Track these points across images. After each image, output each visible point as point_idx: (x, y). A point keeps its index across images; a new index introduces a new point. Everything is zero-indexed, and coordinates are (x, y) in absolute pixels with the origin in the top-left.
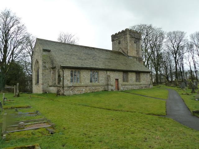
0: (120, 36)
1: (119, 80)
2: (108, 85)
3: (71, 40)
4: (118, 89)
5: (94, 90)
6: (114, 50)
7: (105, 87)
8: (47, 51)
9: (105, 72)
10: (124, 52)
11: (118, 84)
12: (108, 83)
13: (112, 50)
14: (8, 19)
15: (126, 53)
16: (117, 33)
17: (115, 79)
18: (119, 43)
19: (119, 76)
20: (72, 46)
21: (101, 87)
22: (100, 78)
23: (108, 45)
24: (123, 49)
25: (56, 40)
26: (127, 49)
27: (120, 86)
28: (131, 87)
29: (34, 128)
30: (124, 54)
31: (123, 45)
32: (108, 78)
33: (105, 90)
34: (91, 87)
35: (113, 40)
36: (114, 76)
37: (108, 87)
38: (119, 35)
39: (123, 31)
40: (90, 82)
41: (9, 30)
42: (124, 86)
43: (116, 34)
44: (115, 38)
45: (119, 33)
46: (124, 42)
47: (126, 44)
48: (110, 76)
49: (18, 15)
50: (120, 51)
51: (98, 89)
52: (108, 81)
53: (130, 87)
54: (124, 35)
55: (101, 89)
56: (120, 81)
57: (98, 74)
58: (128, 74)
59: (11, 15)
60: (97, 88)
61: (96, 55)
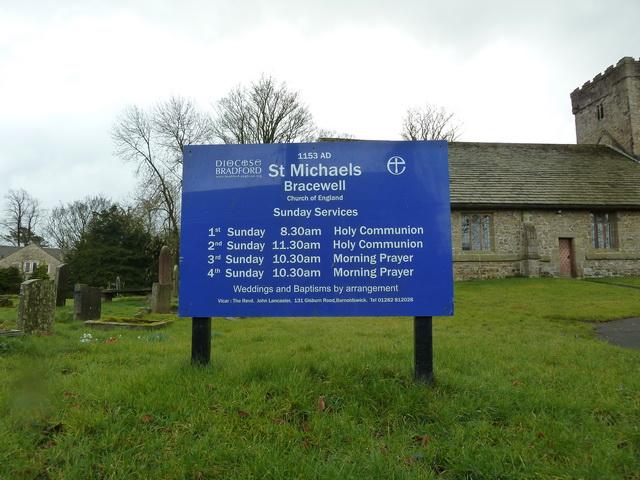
0: (601, 91)
1: (577, 242)
2: (526, 257)
3: (443, 133)
4: (574, 273)
5: (477, 273)
6: (582, 142)
7: (517, 266)
8: (629, 210)
9: (517, 216)
10: (618, 146)
11: (572, 257)
12: (526, 251)
13: (575, 143)
14: (271, 101)
15: (626, 146)
16: (592, 81)
17: (560, 239)
18: (600, 115)
19: (581, 229)
20: (332, 140)
21: (504, 264)
22: (499, 237)
23: (563, 131)
24: (616, 135)
25: (400, 138)
26: (629, 131)
27: (580, 261)
28: (630, 267)
29: (133, 290)
30: (621, 152)
31: (613, 123)
32: (527, 235)
33: (519, 276)
34: (466, 264)
35: (576, 110)
36: (549, 230)
37: (526, 265)
38: (597, 88)
39: (611, 71)
40: (464, 249)
41: (274, 130)
42: (597, 263)
43: (587, 85)
44: (582, 99)
45: (598, 78)
46: (615, 110)
47: (625, 113)
48: (532, 229)
49: (290, 90)
50: (606, 142)
51: (492, 270)
52: (526, 244)
53: (629, 265)
54: (615, 84)
55: (503, 271)
56: (582, 247)
57: (492, 220)
58: (617, 219)
59: (277, 89)
60: (488, 268)
61: (496, 165)
